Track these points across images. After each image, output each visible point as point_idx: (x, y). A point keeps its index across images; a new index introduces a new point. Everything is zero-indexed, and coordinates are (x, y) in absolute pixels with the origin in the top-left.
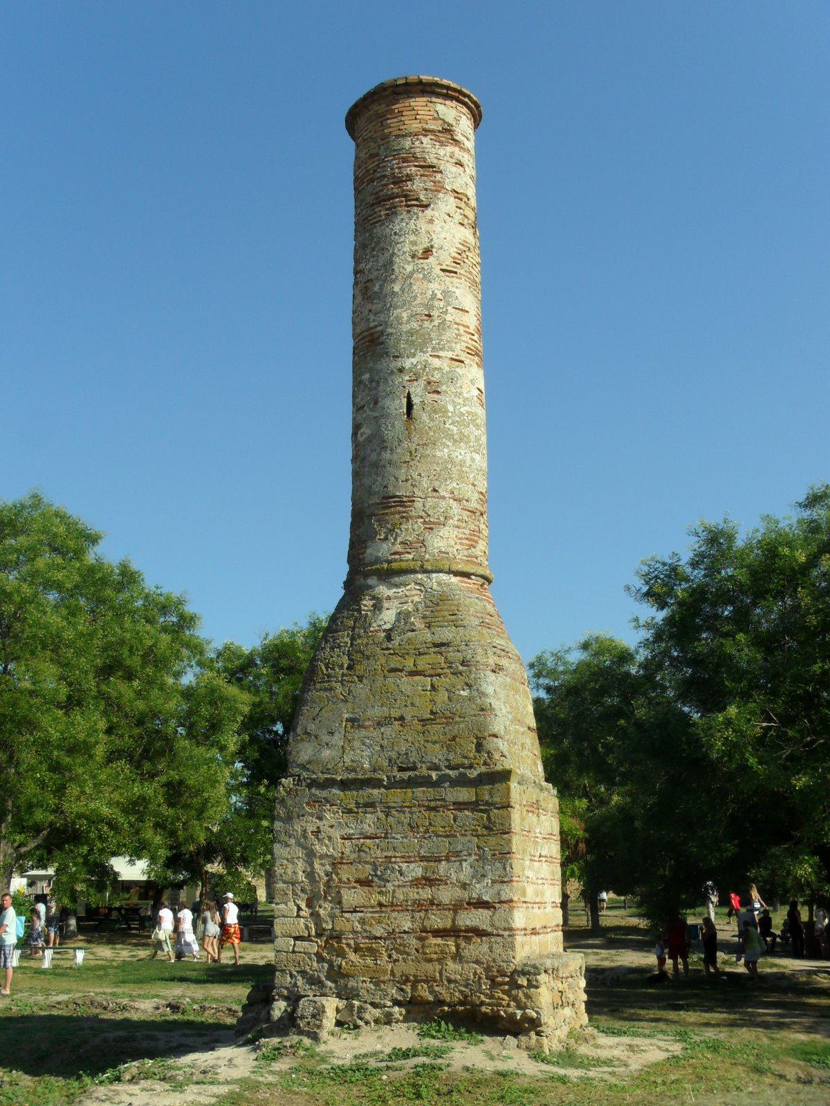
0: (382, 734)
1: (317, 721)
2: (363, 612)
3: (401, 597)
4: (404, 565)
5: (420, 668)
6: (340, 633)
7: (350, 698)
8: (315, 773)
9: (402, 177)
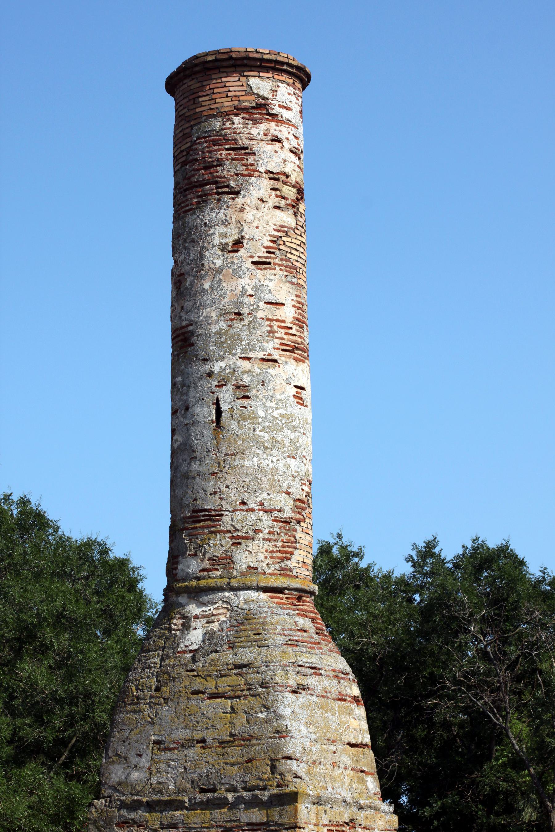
0: (186, 756)
1: (127, 744)
2: (173, 632)
3: (208, 616)
4: (211, 582)
5: (221, 690)
6: (151, 653)
7: (157, 720)
8: (124, 795)
9: (213, 161)
